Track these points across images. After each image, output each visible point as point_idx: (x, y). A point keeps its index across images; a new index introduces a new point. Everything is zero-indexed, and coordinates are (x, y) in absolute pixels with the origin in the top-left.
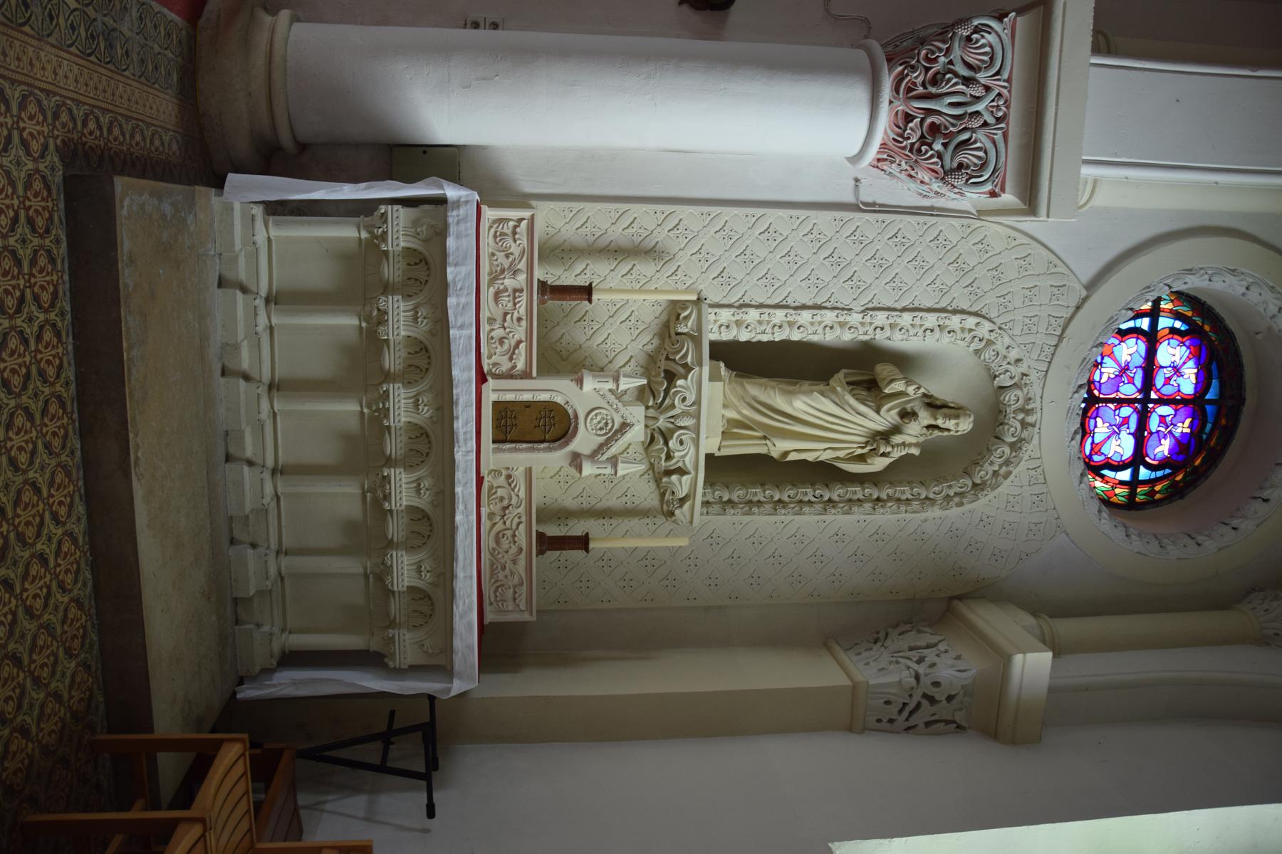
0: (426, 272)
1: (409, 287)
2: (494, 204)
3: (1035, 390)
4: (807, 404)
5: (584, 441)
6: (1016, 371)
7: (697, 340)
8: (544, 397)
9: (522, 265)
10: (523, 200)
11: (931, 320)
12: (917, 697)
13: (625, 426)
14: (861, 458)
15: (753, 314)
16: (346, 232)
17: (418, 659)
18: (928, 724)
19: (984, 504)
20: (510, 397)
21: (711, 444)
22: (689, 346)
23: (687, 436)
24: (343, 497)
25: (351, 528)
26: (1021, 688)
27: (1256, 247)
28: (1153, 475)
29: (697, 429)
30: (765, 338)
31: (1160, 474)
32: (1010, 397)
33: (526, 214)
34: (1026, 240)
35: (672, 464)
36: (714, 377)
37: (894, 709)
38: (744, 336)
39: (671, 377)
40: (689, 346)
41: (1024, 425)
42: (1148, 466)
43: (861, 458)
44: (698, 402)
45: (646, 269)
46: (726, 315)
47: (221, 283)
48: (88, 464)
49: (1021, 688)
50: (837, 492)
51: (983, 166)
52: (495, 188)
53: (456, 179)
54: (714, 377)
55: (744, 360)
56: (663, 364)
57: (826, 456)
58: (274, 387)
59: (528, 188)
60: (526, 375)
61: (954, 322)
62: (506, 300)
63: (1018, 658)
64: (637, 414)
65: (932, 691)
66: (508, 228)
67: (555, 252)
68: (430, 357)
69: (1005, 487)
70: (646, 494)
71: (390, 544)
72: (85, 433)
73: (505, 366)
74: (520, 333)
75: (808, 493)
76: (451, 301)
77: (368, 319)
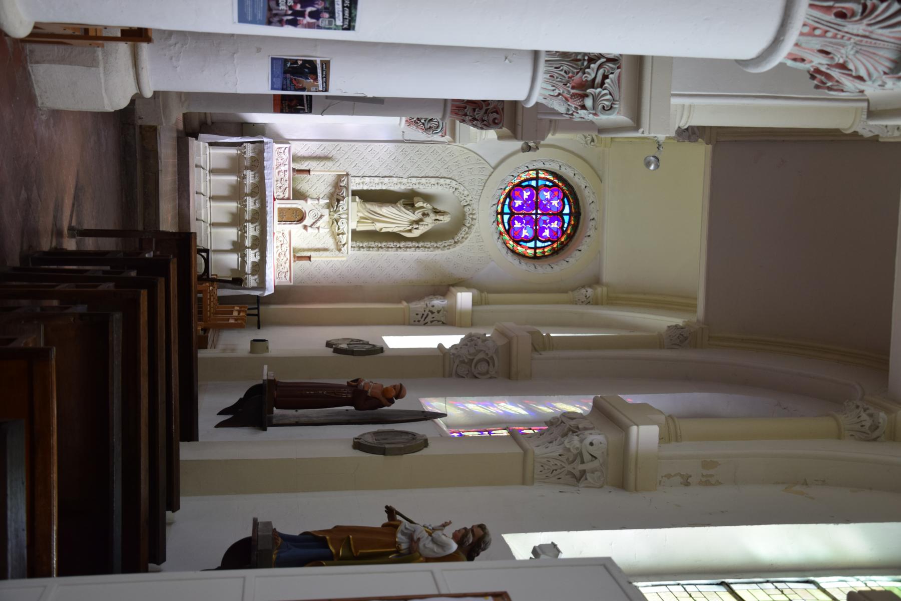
0: (258, 164)
1: (251, 168)
2: (277, 143)
3: (475, 206)
4: (387, 210)
5: (308, 221)
6: (468, 199)
7: (347, 188)
8: (294, 206)
9: (287, 163)
10: (286, 141)
11: (433, 181)
12: (427, 311)
13: (321, 216)
14: (410, 231)
15: (367, 180)
16: (233, 151)
17: (255, 285)
18: (432, 322)
19: (459, 247)
20: (283, 206)
21: (353, 225)
22: (344, 190)
23: (345, 221)
24: (232, 233)
25: (234, 243)
26: (637, 452)
27: (562, 151)
28: (543, 245)
29: (347, 219)
30: (373, 188)
31: (546, 244)
32: (466, 209)
33: (287, 146)
34: (466, 151)
35: (341, 231)
36: (354, 201)
37: (419, 316)
38: (365, 188)
39: (338, 201)
40: (344, 190)
41: (472, 219)
42: (540, 241)
43: (410, 231)
44: (347, 209)
45: (329, 164)
46: (358, 180)
47: (197, 166)
48: (180, 206)
49: (637, 452)
50: (402, 244)
51: (438, 127)
52: (279, 139)
53: (264, 135)
54: (354, 201)
55: (367, 196)
56: (335, 196)
57: (396, 230)
58: (212, 198)
59: (287, 137)
60: (288, 199)
61: (442, 181)
62: (282, 174)
63: (634, 429)
64: (326, 212)
65: (432, 309)
66: (282, 151)
67: (296, 159)
68: (259, 190)
69: (466, 242)
70: (330, 243)
71: (246, 248)
72: (179, 198)
73: (281, 196)
74: (286, 185)
75: (391, 244)
76: (266, 172)
77: (239, 177)
